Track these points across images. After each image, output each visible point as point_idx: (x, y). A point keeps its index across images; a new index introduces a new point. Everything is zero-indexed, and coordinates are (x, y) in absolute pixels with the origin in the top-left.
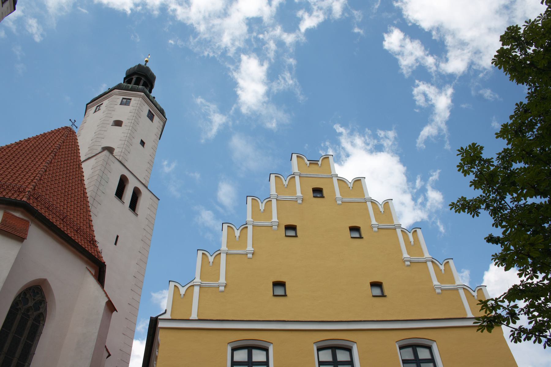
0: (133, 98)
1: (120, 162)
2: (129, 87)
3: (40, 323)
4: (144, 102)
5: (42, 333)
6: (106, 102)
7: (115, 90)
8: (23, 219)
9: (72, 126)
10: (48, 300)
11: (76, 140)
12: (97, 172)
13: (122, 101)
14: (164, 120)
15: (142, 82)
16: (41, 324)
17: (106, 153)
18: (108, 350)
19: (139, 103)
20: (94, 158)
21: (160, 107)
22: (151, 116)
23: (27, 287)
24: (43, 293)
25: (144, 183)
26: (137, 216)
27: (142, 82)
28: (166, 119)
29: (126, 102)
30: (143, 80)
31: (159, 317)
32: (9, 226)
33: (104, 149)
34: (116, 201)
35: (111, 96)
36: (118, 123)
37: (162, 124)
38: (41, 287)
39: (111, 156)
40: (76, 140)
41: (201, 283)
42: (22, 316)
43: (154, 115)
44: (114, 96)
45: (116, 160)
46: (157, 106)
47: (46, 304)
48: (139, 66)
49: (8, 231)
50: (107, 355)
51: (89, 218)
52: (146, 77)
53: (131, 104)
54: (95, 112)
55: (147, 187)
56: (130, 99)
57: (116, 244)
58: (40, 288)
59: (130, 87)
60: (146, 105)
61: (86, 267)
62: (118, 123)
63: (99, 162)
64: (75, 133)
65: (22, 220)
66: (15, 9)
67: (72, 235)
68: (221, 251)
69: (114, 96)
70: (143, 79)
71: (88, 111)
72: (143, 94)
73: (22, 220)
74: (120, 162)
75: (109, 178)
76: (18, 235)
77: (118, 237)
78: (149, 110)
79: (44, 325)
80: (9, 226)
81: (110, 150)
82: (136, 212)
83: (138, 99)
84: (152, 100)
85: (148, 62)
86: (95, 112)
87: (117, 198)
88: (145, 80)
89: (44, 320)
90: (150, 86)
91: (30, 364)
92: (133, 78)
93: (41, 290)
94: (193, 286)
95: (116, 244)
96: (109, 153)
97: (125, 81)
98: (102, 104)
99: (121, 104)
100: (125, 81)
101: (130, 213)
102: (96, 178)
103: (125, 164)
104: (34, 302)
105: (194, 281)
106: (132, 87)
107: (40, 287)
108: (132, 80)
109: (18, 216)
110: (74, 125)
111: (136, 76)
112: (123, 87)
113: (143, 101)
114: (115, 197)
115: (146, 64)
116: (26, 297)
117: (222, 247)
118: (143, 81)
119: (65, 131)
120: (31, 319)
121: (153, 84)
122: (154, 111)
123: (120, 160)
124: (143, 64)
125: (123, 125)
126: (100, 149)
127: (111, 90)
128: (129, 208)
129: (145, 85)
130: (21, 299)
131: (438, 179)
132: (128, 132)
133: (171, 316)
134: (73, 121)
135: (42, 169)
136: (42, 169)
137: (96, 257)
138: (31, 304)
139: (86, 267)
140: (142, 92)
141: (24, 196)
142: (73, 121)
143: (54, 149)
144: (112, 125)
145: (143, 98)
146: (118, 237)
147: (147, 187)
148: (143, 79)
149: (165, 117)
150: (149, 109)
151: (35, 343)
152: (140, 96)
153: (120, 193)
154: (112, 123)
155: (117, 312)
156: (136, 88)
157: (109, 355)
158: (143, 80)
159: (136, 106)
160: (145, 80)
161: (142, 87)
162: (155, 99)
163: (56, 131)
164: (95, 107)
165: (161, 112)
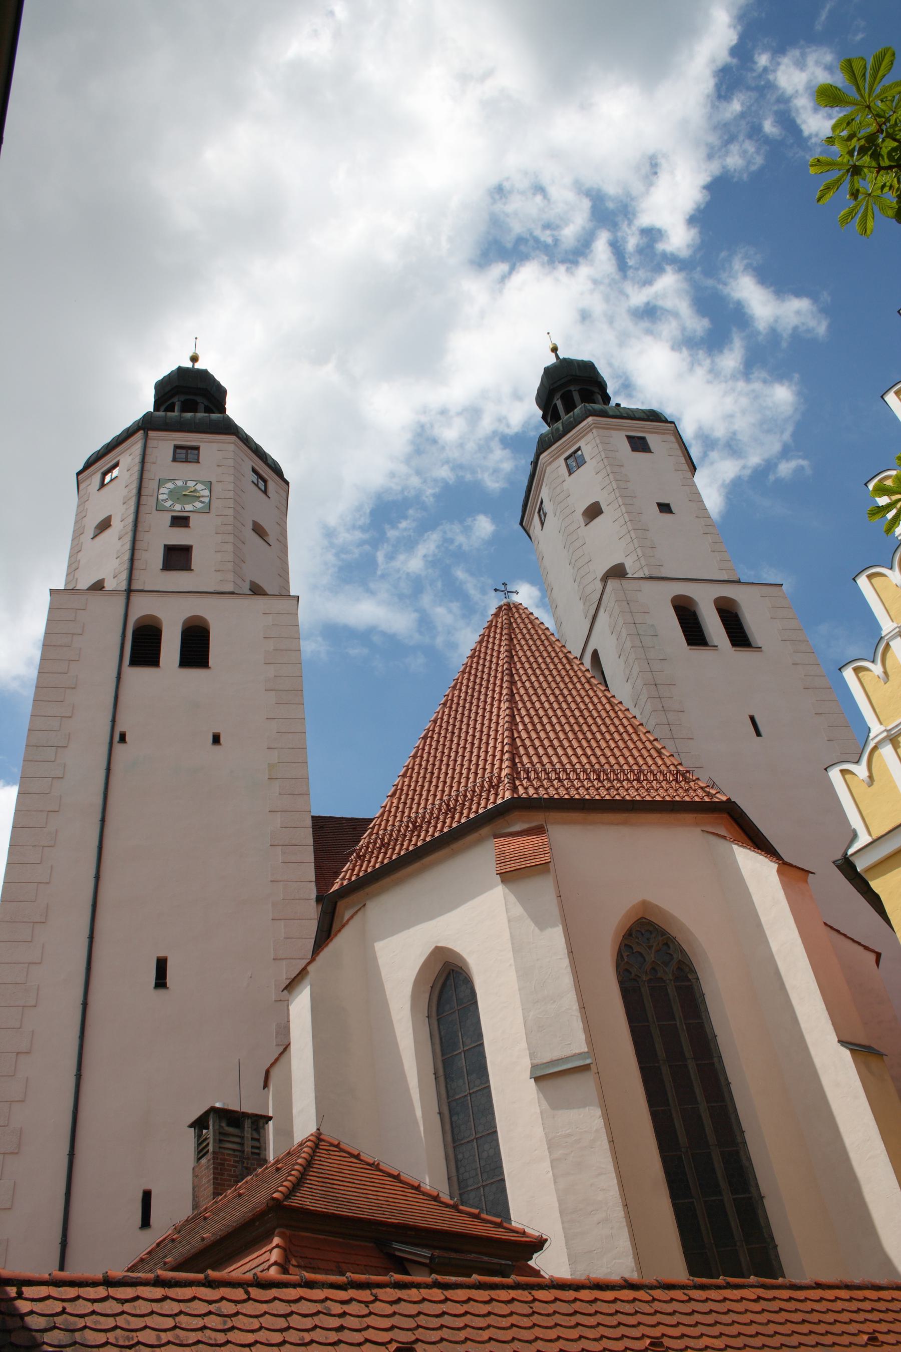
0: (581, 443)
1: (651, 578)
2: (558, 429)
3: (689, 980)
4: (606, 432)
5: (704, 995)
6: (545, 493)
7: (542, 457)
8: (530, 827)
9: (506, 597)
10: (673, 932)
11: (531, 616)
12: (624, 634)
13: (567, 466)
14: (670, 428)
15: (576, 397)
16: (693, 981)
17: (612, 584)
18: (869, 948)
19: (598, 441)
20: (602, 610)
21: (643, 411)
22: (639, 445)
23: (623, 934)
24: (657, 927)
25: (726, 578)
26: (761, 651)
27: (576, 397)
28: (673, 423)
29: (575, 461)
30: (575, 390)
31: (850, 852)
32: (513, 859)
33: (605, 578)
34: (699, 654)
35: (544, 472)
36: (593, 512)
37: (672, 438)
38: (646, 919)
39: (625, 582)
40: (531, 616)
41: (887, 731)
42: (648, 987)
43: (643, 439)
44: (548, 468)
45: (641, 582)
46: (637, 416)
47: (676, 943)
48: (548, 371)
49: (515, 868)
50: (873, 957)
51: (647, 737)
52: (575, 379)
53: (587, 458)
54: (542, 524)
55: (738, 582)
56: (579, 449)
57: (758, 734)
58: (647, 921)
59: (561, 428)
60: (614, 433)
61: (702, 830)
62: (593, 512)
63: (614, 611)
64: (520, 606)
65: (530, 830)
66: (287, 483)
67: (633, 795)
68: (886, 638)
69: (549, 470)
70: (572, 388)
71: (531, 533)
72: (590, 419)
73: (530, 830)
74: (651, 578)
75: (653, 625)
76: (534, 864)
77: (752, 719)
78: (629, 437)
79: (698, 979)
80: (513, 859)
81: (617, 572)
82: (753, 646)
83: (590, 436)
84: (618, 414)
85: (559, 349)
86: (542, 524)
87: (698, 649)
88: (578, 388)
89: (693, 971)
90: (596, 390)
91: (721, 1057)
92: (556, 404)
93: (650, 923)
94: (875, 748)
95: (758, 734)
96: (618, 581)
97: (549, 421)
98: (542, 502)
99: (570, 474)
100: (549, 421)
101: (742, 656)
102: (628, 644)
103: (663, 575)
104: (653, 952)
105: (872, 735)
106: (563, 426)
107: (644, 920)
108: (557, 407)
109: (520, 830)
110: (508, 592)
111: (558, 395)
112: (549, 438)
113: (601, 431)
114: (690, 649)
115: (557, 357)
116: (635, 951)
117: (884, 629)
118: (577, 392)
119: (502, 617)
120: (668, 981)
121: (599, 380)
122: (638, 429)
123: (647, 574)
124: (551, 360)
125: (603, 507)
126: (599, 586)
127: (535, 463)
128: (734, 649)
129: (588, 397)
130: (626, 960)
131: (538, 586)
132: (621, 511)
133: (870, 834)
134: (503, 588)
135: (504, 718)
136: (504, 718)
137: (706, 799)
138: (650, 957)
139: (702, 830)
140: (587, 417)
141: (504, 789)
142: (503, 588)
143: (503, 666)
144: (585, 526)
145: (598, 427)
146: (752, 719)
147: (738, 582)
148: (572, 388)
149: (666, 421)
150: (629, 437)
151: (704, 1017)
152: (589, 429)
154: (581, 520)
155: (814, 873)
156: (572, 419)
157: (878, 956)
158: (575, 390)
159: (598, 452)
160: (578, 388)
161: (581, 408)
162: (622, 406)
163: (488, 630)
164: (536, 514)
165: (652, 421)
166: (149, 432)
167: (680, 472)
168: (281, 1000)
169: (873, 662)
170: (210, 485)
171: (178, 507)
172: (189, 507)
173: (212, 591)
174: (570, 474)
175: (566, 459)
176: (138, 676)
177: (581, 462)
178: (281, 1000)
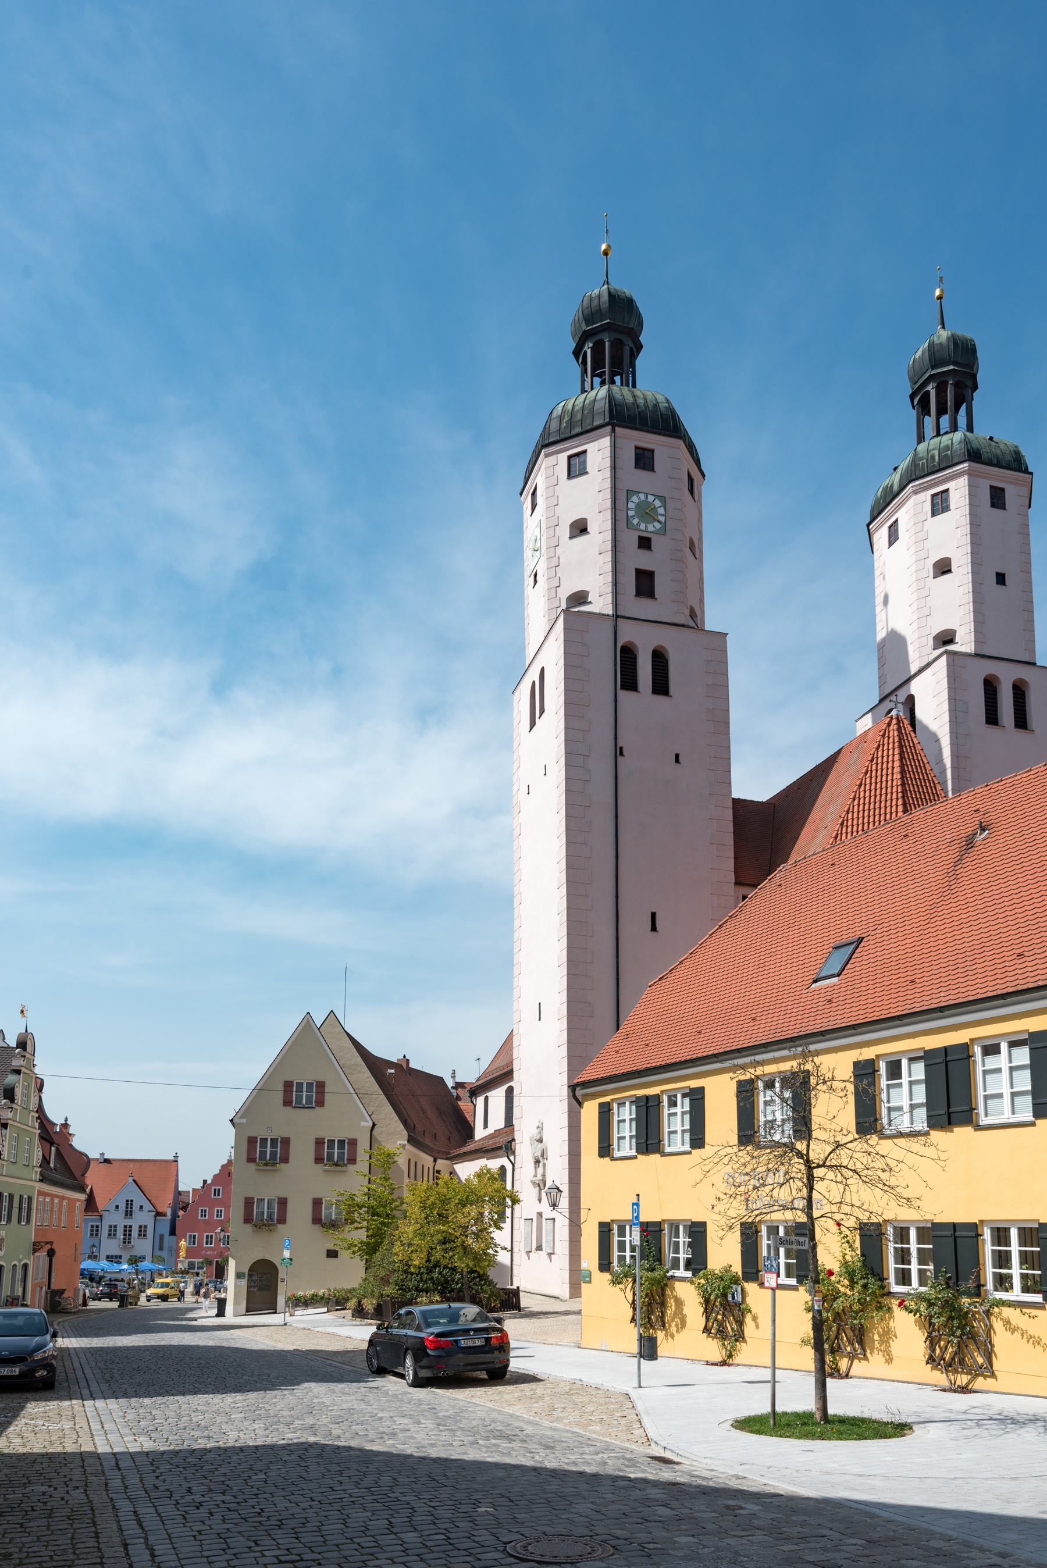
0: (950, 485)
13: (933, 505)
34: (992, 730)
53: (952, 506)
99: (933, 514)
101: (1021, 734)
125: (954, 567)
150: (991, 487)
153: (629, 681)
166: (617, 429)
167: (954, 1427)
168: (619, 752)
169: (998, 1229)
170: (663, 499)
171: (642, 526)
172: (651, 528)
173: (669, 621)
174: (933, 514)
175: (933, 496)
176: (625, 696)
177: (946, 509)
178: (619, 752)
